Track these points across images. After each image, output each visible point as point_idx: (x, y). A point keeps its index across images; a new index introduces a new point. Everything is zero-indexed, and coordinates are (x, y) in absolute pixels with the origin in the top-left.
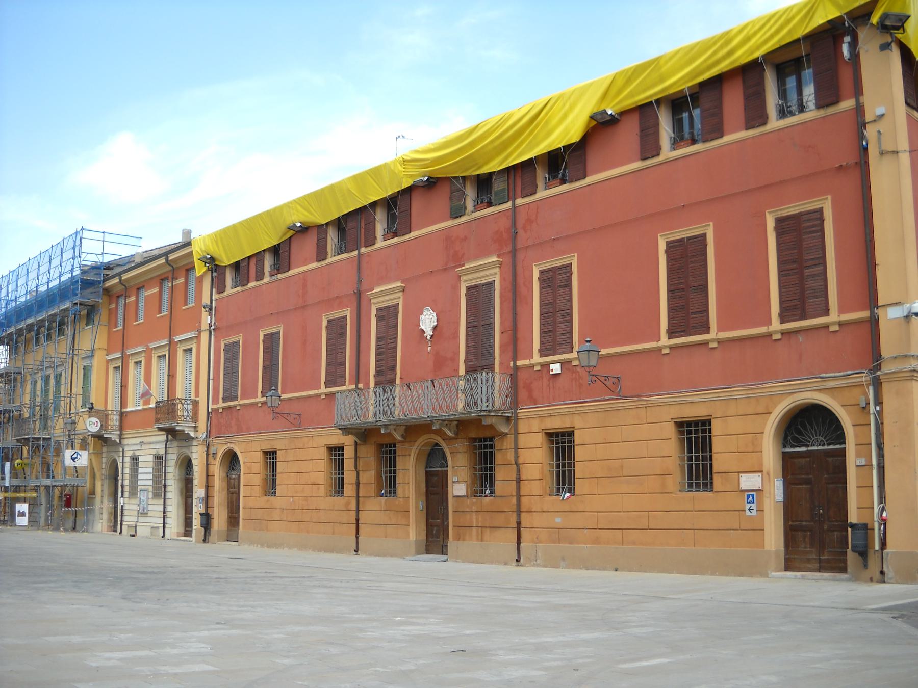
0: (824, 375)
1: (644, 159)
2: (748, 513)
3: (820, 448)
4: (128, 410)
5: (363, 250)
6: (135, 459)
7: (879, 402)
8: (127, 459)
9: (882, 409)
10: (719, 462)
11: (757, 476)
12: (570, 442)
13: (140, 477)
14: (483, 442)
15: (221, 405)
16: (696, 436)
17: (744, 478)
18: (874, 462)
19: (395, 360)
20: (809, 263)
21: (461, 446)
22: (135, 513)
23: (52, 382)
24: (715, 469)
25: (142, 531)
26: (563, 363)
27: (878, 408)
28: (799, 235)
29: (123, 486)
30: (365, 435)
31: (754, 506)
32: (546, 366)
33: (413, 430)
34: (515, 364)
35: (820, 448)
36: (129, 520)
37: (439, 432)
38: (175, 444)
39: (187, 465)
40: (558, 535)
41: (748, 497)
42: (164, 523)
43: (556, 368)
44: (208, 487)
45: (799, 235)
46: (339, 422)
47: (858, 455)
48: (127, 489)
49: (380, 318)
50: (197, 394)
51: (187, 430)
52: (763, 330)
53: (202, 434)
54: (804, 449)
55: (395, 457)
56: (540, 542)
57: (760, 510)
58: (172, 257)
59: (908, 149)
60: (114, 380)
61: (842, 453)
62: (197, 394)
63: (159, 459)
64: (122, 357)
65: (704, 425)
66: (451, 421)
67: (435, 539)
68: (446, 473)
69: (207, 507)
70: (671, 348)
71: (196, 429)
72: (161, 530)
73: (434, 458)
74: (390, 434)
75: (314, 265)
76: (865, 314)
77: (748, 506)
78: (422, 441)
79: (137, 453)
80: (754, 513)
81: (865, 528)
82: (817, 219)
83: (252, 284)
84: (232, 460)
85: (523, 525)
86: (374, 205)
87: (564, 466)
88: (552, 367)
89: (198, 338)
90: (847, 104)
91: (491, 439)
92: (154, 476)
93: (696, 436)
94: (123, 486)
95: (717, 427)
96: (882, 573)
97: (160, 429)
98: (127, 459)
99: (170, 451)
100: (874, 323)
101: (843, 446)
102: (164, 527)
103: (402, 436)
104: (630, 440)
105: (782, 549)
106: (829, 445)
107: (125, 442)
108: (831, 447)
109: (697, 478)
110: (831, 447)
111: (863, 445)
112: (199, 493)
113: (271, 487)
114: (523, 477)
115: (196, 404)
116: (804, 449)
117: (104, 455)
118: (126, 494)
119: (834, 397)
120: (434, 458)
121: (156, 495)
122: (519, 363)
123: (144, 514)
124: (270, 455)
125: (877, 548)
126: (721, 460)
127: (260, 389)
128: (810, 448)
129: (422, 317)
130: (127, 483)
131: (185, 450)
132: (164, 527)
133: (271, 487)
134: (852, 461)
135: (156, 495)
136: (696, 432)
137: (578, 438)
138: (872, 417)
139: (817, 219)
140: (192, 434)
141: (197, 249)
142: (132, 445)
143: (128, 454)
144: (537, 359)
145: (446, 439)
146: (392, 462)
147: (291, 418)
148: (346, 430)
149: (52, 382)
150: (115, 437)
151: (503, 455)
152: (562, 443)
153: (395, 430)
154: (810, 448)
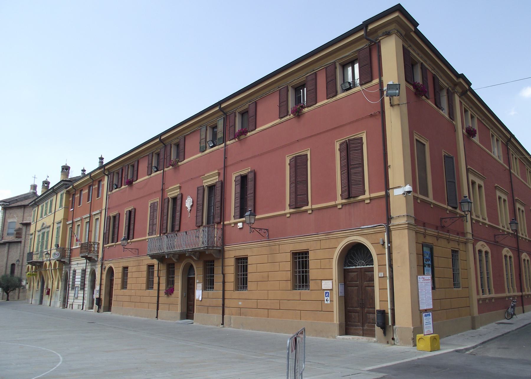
0: (362, 227)
1: (281, 118)
2: (326, 302)
3: (362, 267)
5: (166, 169)
6: (75, 271)
7: (390, 241)
8: (72, 272)
9: (391, 245)
12: (306, 257)
16: (301, 260)
17: (324, 282)
18: (388, 275)
20: (353, 166)
23: (46, 234)
24: (249, 280)
25: (75, 307)
26: (243, 222)
27: (389, 245)
28: (351, 150)
30: (161, 258)
31: (329, 299)
32: (236, 224)
33: (181, 256)
34: (223, 223)
35: (362, 267)
36: (70, 301)
37: (190, 257)
38: (90, 264)
39: (93, 274)
40: (241, 311)
41: (326, 293)
43: (240, 225)
44: (101, 285)
45: (351, 150)
47: (379, 271)
48: (71, 286)
50: (99, 241)
52: (333, 203)
54: (354, 267)
55: (247, 266)
56: (232, 315)
59: (405, 102)
61: (372, 270)
63: (84, 271)
64: (90, 216)
66: (196, 252)
73: (189, 270)
74: (170, 259)
75: (278, 121)
76: (383, 193)
77: (326, 298)
80: (329, 302)
81: (383, 313)
82: (359, 143)
83: (341, 95)
84: (111, 271)
85: (225, 306)
87: (303, 272)
89: (101, 213)
90: (376, 81)
91: (213, 262)
92: (82, 280)
93: (301, 260)
95: (311, 255)
96: (393, 339)
97: (82, 257)
98: (72, 272)
100: (387, 196)
101: (371, 266)
102: (83, 305)
103: (177, 260)
104: (269, 262)
105: (344, 322)
106: (366, 265)
107: (72, 263)
108: (368, 266)
109: (303, 283)
110: (368, 266)
111: (381, 266)
112: (97, 288)
113: (124, 285)
114: (226, 281)
115: (99, 244)
116: (354, 267)
118: (70, 289)
119: (367, 239)
120: (189, 270)
121: (81, 289)
122: (225, 223)
124: (125, 269)
125: (390, 324)
126: (313, 273)
128: (358, 267)
129: (187, 201)
131: (94, 267)
132: (83, 305)
133: (124, 285)
134: (377, 274)
135: (81, 289)
136: (303, 258)
137: (249, 261)
138: (386, 249)
139: (359, 143)
140: (96, 259)
143: (72, 269)
144: (233, 221)
145: (194, 260)
146: (212, 271)
147: (262, 232)
148: (153, 257)
149: (46, 234)
151: (218, 270)
152: (242, 263)
153: (173, 256)
154: (358, 267)
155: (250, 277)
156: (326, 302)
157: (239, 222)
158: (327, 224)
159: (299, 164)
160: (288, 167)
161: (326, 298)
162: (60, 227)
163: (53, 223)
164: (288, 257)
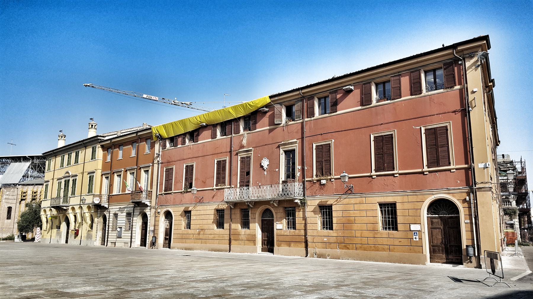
1: (412, 95)
2: (414, 239)
4: (113, 194)
5: (306, 119)
8: (111, 215)
10: (400, 219)
11: (422, 227)
13: (118, 222)
14: (290, 209)
15: (163, 192)
16: (390, 211)
19: (192, 179)
21: (281, 210)
22: (115, 237)
29: (109, 226)
31: (417, 237)
32: (319, 181)
33: (257, 204)
38: (138, 208)
42: (131, 241)
46: (226, 200)
49: (242, 162)
51: (146, 203)
53: (153, 204)
57: (421, 239)
58: (139, 134)
60: (105, 182)
62: (151, 188)
65: (393, 205)
67: (269, 245)
68: (273, 220)
69: (154, 234)
70: (377, 176)
71: (151, 202)
72: (129, 244)
75: (210, 140)
77: (414, 237)
78: (263, 207)
79: (117, 212)
80: (417, 239)
84: (168, 215)
86: (239, 118)
88: (322, 181)
90: (458, 87)
91: (295, 207)
94: (109, 226)
97: (133, 202)
98: (111, 215)
99: (135, 211)
102: (131, 243)
117: (99, 213)
118: (110, 229)
119: (454, 196)
123: (119, 237)
127: (215, 183)
130: (110, 224)
132: (131, 243)
140: (149, 204)
141: (154, 131)
142: (114, 209)
145: (274, 207)
150: (106, 206)
155: (399, 221)
156: (414, 239)
157: (323, 179)
158: (415, 182)
159: (189, 169)
160: (216, 165)
161: (414, 237)
162: (61, 182)
163: (53, 179)
164: (213, 212)
